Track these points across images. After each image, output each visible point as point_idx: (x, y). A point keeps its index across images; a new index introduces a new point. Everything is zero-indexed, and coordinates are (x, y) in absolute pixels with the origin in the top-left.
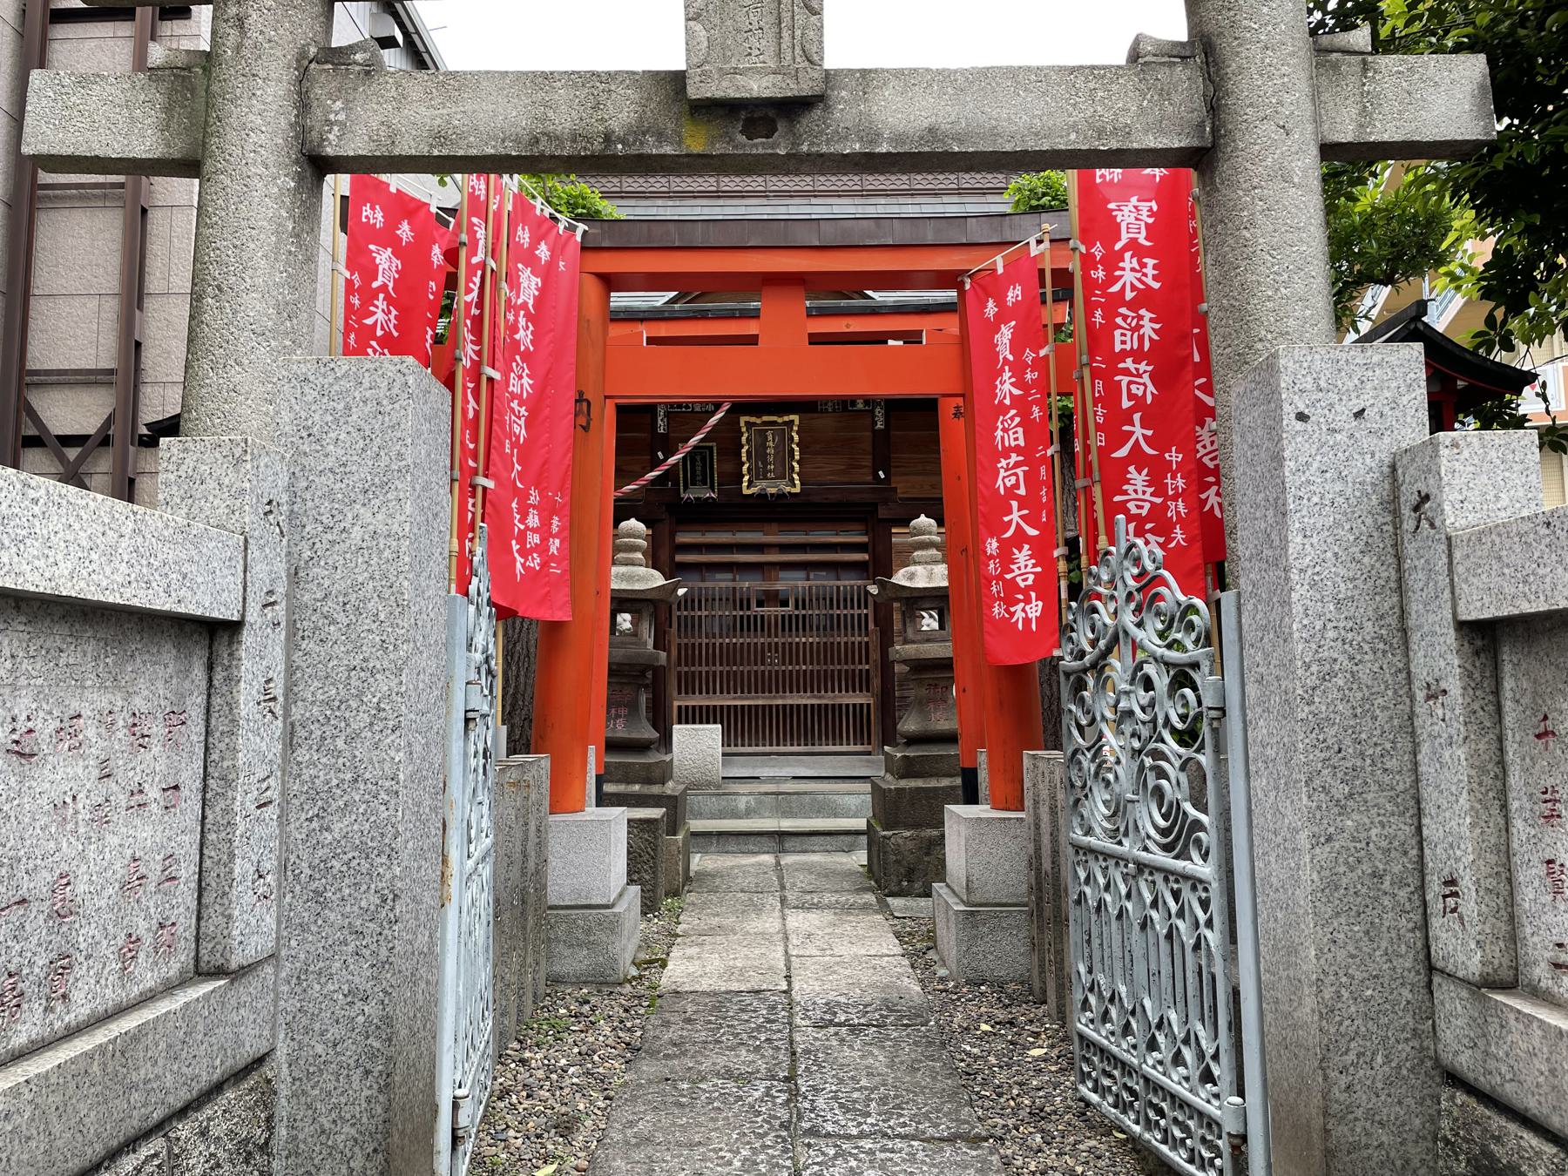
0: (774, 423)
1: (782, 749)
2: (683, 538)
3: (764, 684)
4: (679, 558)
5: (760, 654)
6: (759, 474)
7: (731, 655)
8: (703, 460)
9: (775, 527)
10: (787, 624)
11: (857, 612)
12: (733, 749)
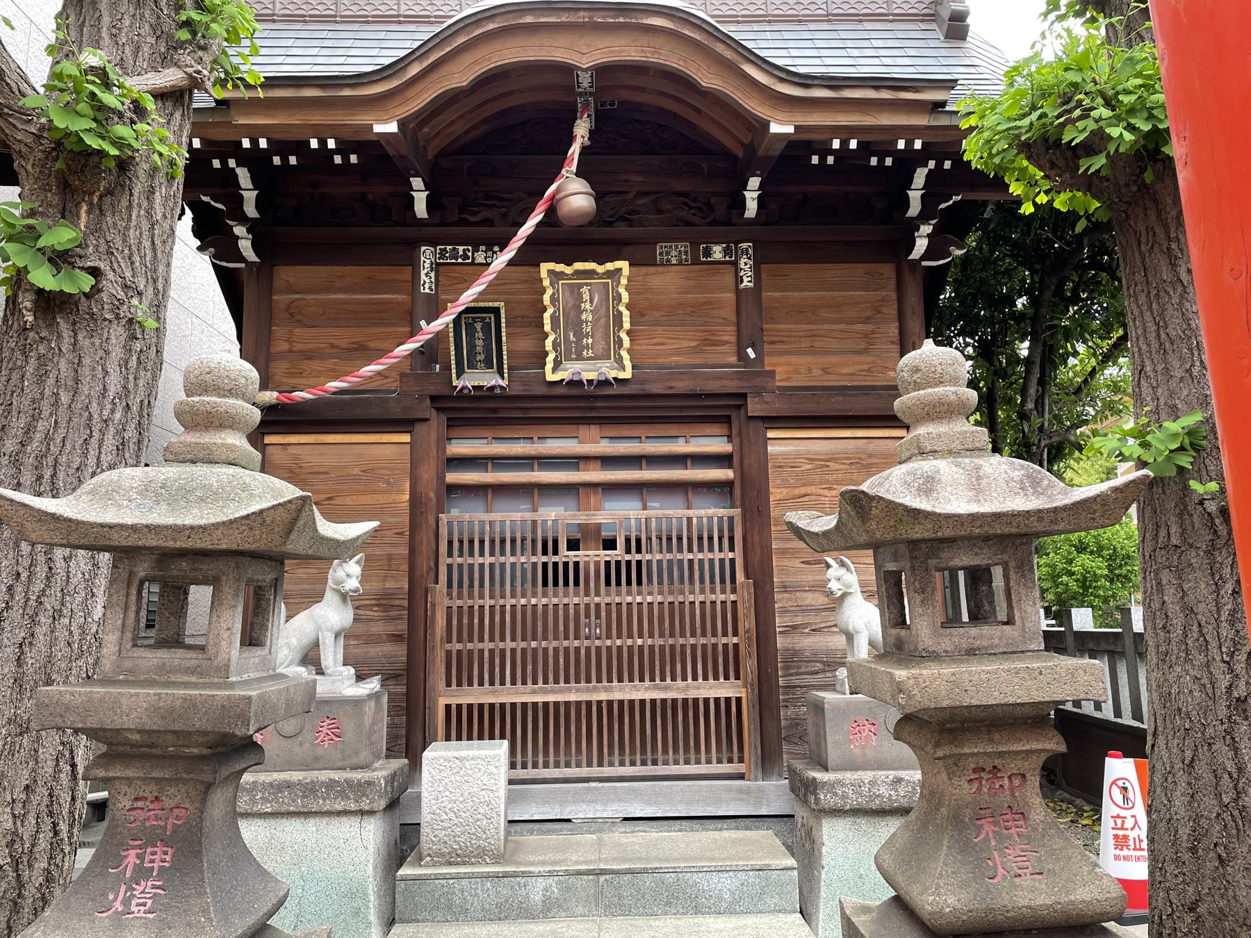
1: (607, 771)
2: (460, 448)
4: (452, 477)
5: (572, 622)
7: (529, 624)
9: (594, 430)
10: (614, 575)
11: (717, 556)
12: (520, 773)
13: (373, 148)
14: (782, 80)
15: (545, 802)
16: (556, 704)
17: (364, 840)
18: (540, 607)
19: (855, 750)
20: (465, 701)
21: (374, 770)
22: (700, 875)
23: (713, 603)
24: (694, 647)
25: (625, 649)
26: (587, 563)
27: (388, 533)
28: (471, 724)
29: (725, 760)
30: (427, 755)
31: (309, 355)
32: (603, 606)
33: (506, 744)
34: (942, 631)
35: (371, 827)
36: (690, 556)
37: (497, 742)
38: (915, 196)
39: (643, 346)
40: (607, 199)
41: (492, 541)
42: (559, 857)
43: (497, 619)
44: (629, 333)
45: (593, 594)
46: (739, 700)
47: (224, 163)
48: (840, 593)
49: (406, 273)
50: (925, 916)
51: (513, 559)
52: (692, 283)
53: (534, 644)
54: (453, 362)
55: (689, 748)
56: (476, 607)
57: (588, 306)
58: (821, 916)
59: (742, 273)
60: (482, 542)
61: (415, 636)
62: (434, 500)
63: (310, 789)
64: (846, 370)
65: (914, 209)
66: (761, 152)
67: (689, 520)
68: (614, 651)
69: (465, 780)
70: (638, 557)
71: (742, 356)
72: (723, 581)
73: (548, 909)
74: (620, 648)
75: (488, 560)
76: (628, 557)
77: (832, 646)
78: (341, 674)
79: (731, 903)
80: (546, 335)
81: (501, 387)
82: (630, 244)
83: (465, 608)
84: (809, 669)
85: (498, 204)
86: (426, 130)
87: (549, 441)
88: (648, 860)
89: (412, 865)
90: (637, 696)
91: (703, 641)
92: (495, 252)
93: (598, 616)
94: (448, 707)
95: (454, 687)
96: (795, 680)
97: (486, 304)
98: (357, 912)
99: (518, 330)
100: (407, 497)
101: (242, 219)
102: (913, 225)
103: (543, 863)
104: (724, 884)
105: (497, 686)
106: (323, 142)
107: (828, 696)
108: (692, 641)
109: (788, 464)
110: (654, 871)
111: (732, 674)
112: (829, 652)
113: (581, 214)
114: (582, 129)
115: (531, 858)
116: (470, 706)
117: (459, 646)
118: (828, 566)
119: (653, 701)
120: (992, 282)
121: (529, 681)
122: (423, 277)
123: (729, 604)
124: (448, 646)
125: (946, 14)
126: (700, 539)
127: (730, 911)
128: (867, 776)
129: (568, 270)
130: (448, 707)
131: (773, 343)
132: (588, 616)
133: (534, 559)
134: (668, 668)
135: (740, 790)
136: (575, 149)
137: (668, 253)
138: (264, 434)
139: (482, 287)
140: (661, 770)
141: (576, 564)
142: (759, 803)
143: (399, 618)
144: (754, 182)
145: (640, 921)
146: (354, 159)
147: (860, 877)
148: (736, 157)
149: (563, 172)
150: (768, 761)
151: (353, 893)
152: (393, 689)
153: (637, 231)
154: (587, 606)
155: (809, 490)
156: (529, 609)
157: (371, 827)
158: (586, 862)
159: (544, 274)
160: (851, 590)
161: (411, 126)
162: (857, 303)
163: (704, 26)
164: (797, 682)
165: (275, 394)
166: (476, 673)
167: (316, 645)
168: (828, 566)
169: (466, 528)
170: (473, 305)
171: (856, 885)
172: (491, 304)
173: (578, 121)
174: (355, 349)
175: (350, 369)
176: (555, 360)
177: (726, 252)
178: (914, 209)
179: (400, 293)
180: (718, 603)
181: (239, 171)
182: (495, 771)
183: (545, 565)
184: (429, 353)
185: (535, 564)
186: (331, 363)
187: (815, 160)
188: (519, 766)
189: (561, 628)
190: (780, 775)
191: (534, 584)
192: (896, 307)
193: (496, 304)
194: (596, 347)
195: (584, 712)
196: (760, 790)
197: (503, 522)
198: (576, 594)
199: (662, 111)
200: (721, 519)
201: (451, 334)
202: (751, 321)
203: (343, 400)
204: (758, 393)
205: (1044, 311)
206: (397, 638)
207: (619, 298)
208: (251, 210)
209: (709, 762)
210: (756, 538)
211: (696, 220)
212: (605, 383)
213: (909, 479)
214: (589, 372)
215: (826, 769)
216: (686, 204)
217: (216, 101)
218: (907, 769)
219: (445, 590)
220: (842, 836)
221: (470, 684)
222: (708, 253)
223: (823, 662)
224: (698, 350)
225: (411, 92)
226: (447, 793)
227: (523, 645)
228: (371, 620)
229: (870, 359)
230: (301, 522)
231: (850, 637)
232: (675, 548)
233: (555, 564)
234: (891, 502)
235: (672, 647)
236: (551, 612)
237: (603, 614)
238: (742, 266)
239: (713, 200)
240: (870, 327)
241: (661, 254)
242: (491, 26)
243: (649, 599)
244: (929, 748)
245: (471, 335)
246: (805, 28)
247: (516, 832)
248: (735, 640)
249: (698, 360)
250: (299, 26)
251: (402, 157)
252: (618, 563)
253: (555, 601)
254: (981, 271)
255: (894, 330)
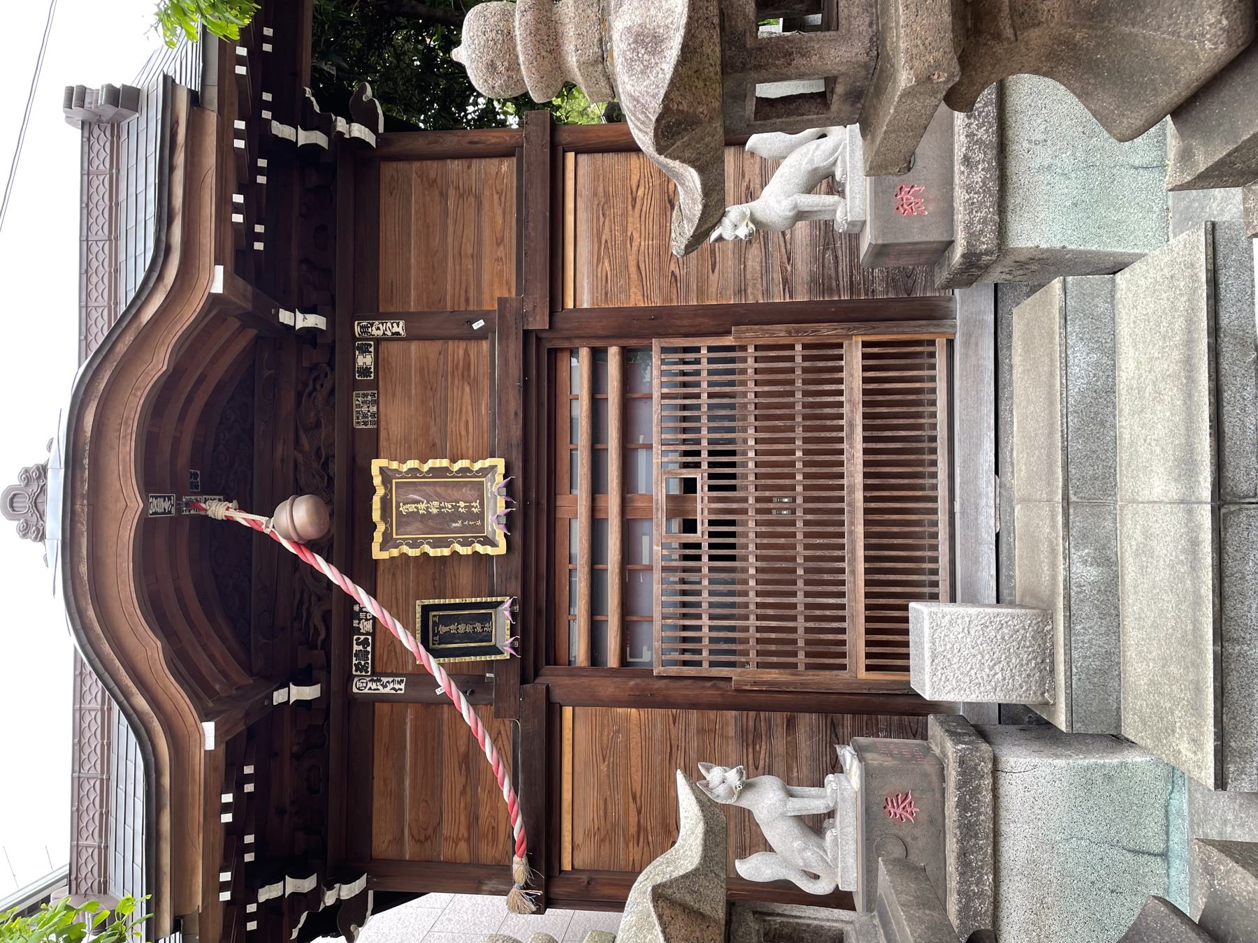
0: (386, 503)
1: (942, 492)
2: (580, 651)
3: (827, 524)
4: (612, 660)
5: (776, 529)
6: (474, 525)
7: (777, 576)
8: (445, 620)
9: (562, 501)
10: (723, 482)
11: (704, 365)
12: (943, 588)
13: (234, 751)
14: (160, 278)
15: (976, 561)
16: (867, 547)
17: (1028, 773)
18: (759, 564)
19: (929, 210)
20: (861, 649)
21: (945, 755)
22: (1070, 387)
23: (756, 371)
24: (805, 394)
25: (807, 470)
26: (711, 511)
27: (673, 732)
28: (890, 641)
29: (932, 361)
30: (927, 696)
31: (473, 820)
32: (758, 494)
33: (913, 605)
34: (843, 30)
35: (1012, 760)
36: (704, 396)
37: (911, 615)
38: (304, 137)
39: (469, 445)
40: (302, 482)
41: (685, 616)
42: (1045, 547)
43: (771, 612)
44: (454, 461)
45: (745, 505)
46: (865, 344)
47: (251, 917)
48: (751, 225)
49: (382, 709)
50: (1234, 51)
51: (705, 594)
52: (398, 390)
53: (800, 572)
54: (483, 658)
55: (918, 400)
56: (758, 635)
57: (422, 506)
58: (1120, 250)
59: (389, 333)
60: (685, 628)
61: (790, 704)
62: (638, 681)
63: (968, 830)
64: (500, 220)
65: (319, 138)
66: (249, 306)
67: (664, 396)
68: (809, 482)
69: (955, 654)
70: (704, 454)
71: (481, 335)
72: (732, 360)
73: (1108, 561)
74: (806, 476)
75: (705, 621)
76: (705, 466)
77: (806, 241)
78: (834, 791)
79: (1103, 352)
80: (455, 553)
81: (512, 604)
82: (354, 459)
83: (759, 647)
84: (832, 266)
85: (305, 606)
86: (217, 687)
87: (573, 551)
88: (1051, 446)
89: (1053, 714)
90: (859, 457)
91: (799, 383)
92: (361, 609)
93: (769, 500)
94: (869, 668)
95: (846, 661)
96: (844, 282)
97: (418, 620)
98: (1109, 778)
99: (449, 585)
100: (634, 710)
101: (317, 894)
102: (337, 139)
103: (1053, 565)
104: (1081, 359)
105: (846, 613)
106: (226, 808)
107: (867, 241)
108: (799, 395)
109: (602, 285)
110: (1065, 439)
111: (836, 352)
112: (813, 242)
113: (316, 512)
114: (219, 510)
115: (1045, 578)
116: (868, 643)
117: (801, 655)
118: (720, 238)
119: (865, 439)
120: (408, 73)
121: (841, 577)
122: (387, 690)
123: (759, 354)
124: (801, 667)
125: (110, 111)
126: (685, 385)
127: (1111, 352)
128: (960, 195)
129: (381, 528)
130: (869, 668)
131: (467, 300)
132: (769, 511)
133: (705, 570)
134: (829, 423)
135: (966, 344)
136: (242, 518)
137: (365, 416)
138: (561, 871)
139: (399, 626)
140: (942, 432)
141: (711, 523)
142: (982, 323)
143: (769, 722)
144: (285, 317)
145: (1123, 456)
146: (249, 770)
147: (1075, 205)
148: (257, 339)
149: (267, 531)
150: (935, 312)
151: (1087, 782)
152: (848, 730)
153: (339, 451)
154: (758, 511)
155: (632, 263)
156: (761, 576)
157: (1012, 760)
158: (1053, 517)
159: (384, 555)
160: (748, 213)
161: (211, 705)
162: (424, 206)
163: (95, 366)
164: (846, 279)
165: (516, 859)
166: (831, 637)
167: (800, 819)
168: (720, 238)
169: (670, 646)
170: (418, 636)
171: (1085, 210)
172: (418, 615)
173: (210, 513)
174: (468, 769)
175: (489, 774)
176: (483, 544)
177: (364, 350)
178: (319, 138)
179: (405, 717)
180: (757, 365)
181: (262, 899)
182: (948, 618)
183: (712, 558)
184: (472, 684)
185: (711, 569)
186: (483, 795)
187: (259, 246)
188: (935, 590)
189: (782, 541)
190: (950, 300)
191: (732, 570)
192: (429, 163)
193: (419, 609)
194: (470, 498)
195: (877, 517)
196: (966, 322)
197: (664, 605)
198: (745, 523)
199: (203, 420)
200: (663, 362)
201: (452, 660)
202: (442, 324)
203: (524, 783)
204: (523, 317)
205: (439, 13)
206: (791, 725)
207: (414, 471)
208: (308, 884)
209: (933, 379)
210: (685, 322)
211: (328, 385)
212: (509, 487)
213: (638, 67)
214: (496, 506)
215: (950, 243)
216: (310, 395)
217: (174, 931)
218: (952, 150)
219: (739, 670)
220: (1028, 226)
221: (843, 643)
222: (365, 371)
223: (825, 250)
224: (474, 384)
225: (169, 707)
226: (973, 672)
227: (800, 583)
228: (771, 754)
229: (487, 193)
230: (689, 899)
231: (800, 215)
232: (696, 413)
233: (711, 546)
234: (672, 82)
235: (805, 417)
236: (765, 552)
237: (767, 494)
238: (380, 333)
239: (306, 364)
240: (452, 192)
241: (365, 424)
242: (91, 613)
243: (751, 442)
244: (999, 49)
245: (451, 638)
246: (123, 266)
247: (1010, 595)
248: (798, 347)
249: (485, 383)
250: (112, 820)
251: (247, 714)
252: (711, 476)
253: (752, 547)
254: (395, 83)
255: (455, 166)
